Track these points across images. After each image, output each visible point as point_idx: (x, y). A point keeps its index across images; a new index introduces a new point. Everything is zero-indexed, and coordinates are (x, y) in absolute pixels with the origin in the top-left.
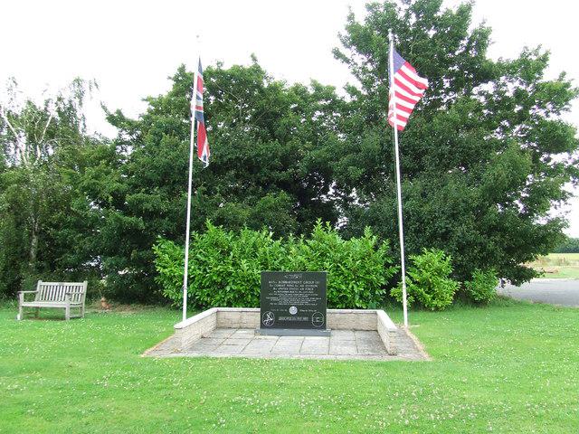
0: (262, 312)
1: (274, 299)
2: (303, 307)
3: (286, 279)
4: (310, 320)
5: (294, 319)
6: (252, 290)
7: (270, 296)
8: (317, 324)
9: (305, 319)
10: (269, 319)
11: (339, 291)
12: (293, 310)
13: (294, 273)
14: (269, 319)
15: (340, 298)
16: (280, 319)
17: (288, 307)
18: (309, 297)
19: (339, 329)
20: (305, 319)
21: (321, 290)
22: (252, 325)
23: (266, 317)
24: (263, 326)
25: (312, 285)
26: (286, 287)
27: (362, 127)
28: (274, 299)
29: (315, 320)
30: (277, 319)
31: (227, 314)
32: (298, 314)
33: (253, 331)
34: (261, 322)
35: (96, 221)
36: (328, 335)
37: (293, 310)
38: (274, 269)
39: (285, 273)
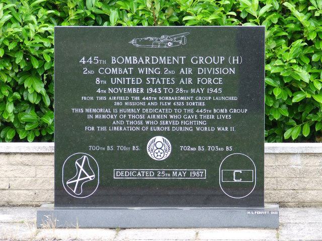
0: (59, 155)
1: (100, 113)
2: (193, 138)
3: (132, 52)
4: (213, 176)
5: (163, 175)
6: (17, 87)
7: (87, 104)
8: (229, 187)
9: (198, 174)
10: (83, 175)
11: (292, 86)
12: (159, 148)
13: (147, 32)
14: (83, 175)
15: (292, 108)
16: (119, 174)
17: (143, 138)
18: (210, 105)
19: (302, 205)
20: (198, 174)
21: (250, 82)
22: (22, 196)
23: (71, 172)
24: (62, 198)
25: (220, 66)
26: (135, 74)
27: (173, 6)
28: (100, 113)
29: (228, 176)
30: (106, 173)
31: (296, 161)
32: (174, 161)
33: (29, 215)
34: (58, 187)
35: (7, 113)
36: (274, 225)
37: (159, 148)
38: (87, 19)
39: (122, 33)
